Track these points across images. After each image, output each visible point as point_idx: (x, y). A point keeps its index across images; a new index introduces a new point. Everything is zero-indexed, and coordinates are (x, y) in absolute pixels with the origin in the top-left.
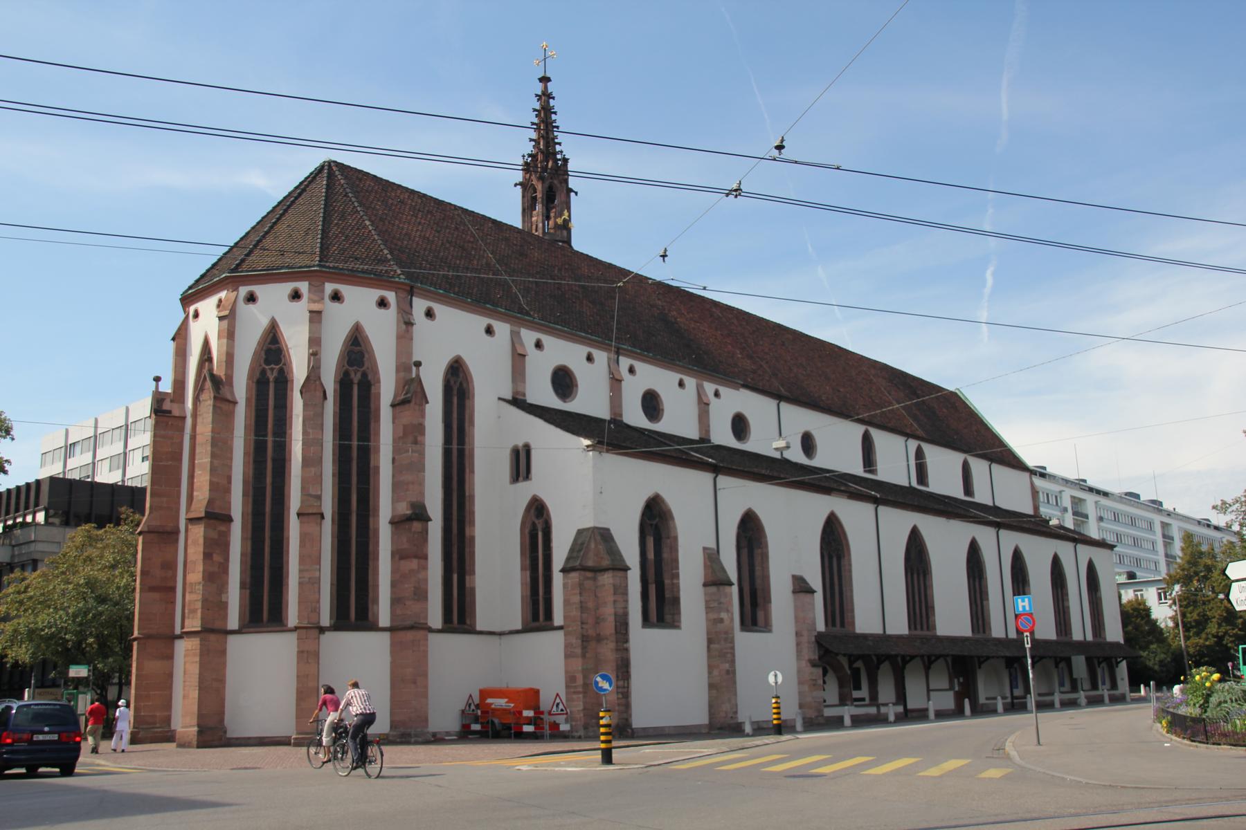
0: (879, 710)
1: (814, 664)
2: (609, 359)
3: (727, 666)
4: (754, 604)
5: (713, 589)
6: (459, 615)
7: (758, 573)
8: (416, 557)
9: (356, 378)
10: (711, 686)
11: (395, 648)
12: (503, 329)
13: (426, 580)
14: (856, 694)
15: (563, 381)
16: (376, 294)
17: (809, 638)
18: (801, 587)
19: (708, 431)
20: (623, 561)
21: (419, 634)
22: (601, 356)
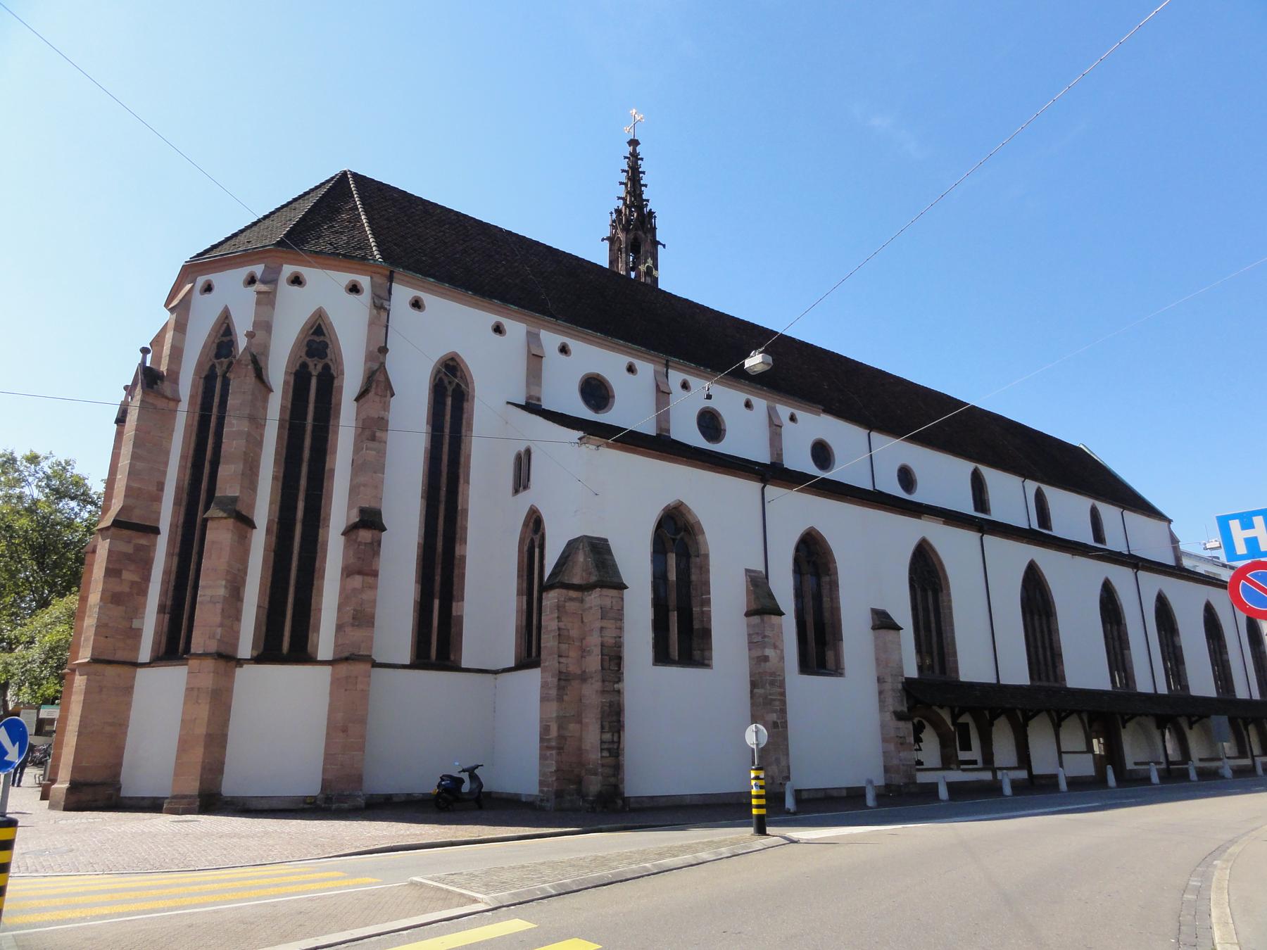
0: (995, 775)
1: (899, 716)
2: (656, 372)
5: (756, 619)
6: (437, 645)
8: (360, 573)
9: (315, 369)
12: (516, 329)
13: (374, 602)
14: (963, 755)
15: (596, 391)
16: (346, 278)
17: (893, 685)
18: (882, 622)
19: (780, 455)
20: (619, 576)
21: (361, 668)
22: (646, 369)
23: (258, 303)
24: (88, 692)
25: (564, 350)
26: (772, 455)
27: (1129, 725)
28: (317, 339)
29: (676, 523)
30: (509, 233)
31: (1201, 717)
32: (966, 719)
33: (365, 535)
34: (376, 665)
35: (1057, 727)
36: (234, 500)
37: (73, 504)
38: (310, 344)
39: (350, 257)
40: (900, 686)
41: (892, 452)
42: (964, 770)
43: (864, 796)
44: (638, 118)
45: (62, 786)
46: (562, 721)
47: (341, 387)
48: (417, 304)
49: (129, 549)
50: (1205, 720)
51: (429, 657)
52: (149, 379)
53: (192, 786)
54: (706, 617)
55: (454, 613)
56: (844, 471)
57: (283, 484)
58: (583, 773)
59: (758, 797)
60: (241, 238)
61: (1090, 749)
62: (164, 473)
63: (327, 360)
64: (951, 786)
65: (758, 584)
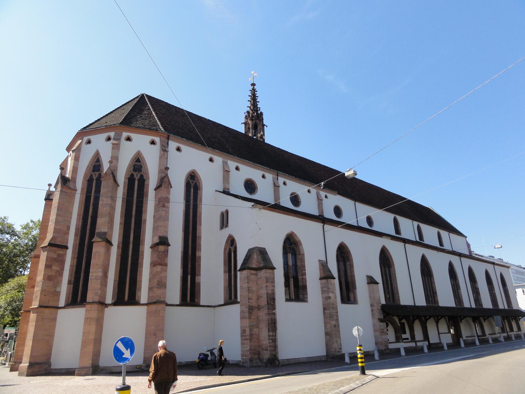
0: (416, 344)
1: (381, 320)
3: (334, 322)
4: (348, 290)
5: (324, 281)
6: (190, 296)
7: (349, 274)
8: (160, 264)
9: (137, 177)
10: (327, 334)
11: (149, 314)
12: (218, 160)
13: (166, 277)
16: (150, 138)
17: (378, 307)
18: (371, 281)
19: (322, 212)
20: (271, 263)
21: (161, 306)
22: (270, 176)
23: (113, 148)
24: (37, 321)
25: (237, 169)
26: (319, 212)
27: (463, 321)
28: (137, 164)
29: (290, 241)
30: (209, 120)
31: (488, 317)
32: (404, 321)
33: (162, 248)
34: (167, 305)
35: (437, 322)
36: (105, 233)
37: (8, 236)
38: (134, 166)
39: (151, 129)
40: (380, 308)
41: (365, 211)
42: (405, 342)
43: (373, 355)
44: (255, 75)
45: (25, 365)
46: (251, 328)
47: (148, 185)
48: (178, 149)
49: (55, 256)
50: (491, 318)
51: (186, 301)
52: (64, 180)
53: (88, 363)
54: (304, 280)
55: (196, 282)
56: (348, 218)
57: (124, 225)
58: (260, 350)
59: (361, 358)
60: (102, 121)
61: (450, 332)
62: (70, 222)
63: (142, 173)
64: (405, 349)
65: (324, 265)
